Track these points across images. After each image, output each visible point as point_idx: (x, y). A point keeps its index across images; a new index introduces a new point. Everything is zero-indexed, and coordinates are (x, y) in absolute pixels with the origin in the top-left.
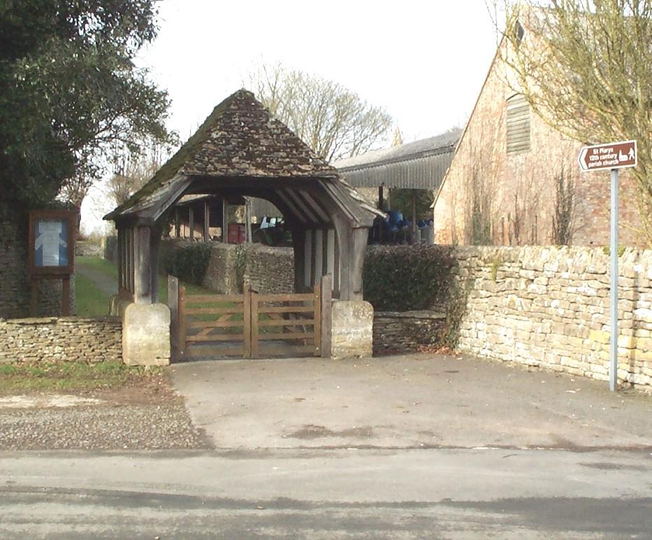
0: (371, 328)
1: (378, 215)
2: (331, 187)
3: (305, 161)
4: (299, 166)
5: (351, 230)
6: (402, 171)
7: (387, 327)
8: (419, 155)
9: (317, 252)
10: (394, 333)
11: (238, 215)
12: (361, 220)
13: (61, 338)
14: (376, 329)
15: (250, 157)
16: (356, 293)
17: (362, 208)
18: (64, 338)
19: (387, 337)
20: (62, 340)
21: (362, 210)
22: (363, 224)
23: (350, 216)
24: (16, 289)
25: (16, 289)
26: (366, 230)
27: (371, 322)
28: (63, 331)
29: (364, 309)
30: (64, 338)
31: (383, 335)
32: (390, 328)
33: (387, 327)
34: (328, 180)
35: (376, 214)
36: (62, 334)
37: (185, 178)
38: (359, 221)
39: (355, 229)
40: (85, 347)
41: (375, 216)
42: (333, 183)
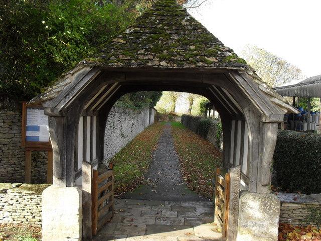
0: (278, 221)
1: (289, 111)
2: (239, 79)
3: (214, 55)
4: (206, 58)
5: (261, 124)
6: (304, 89)
7: (295, 212)
8: (313, 82)
9: (237, 142)
10: (300, 218)
11: (77, 110)
12: (270, 115)
13: (10, 205)
14: (283, 214)
15: (158, 50)
16: (265, 185)
17: (272, 102)
18: (12, 205)
19: (294, 221)
20: (10, 206)
21: (272, 105)
22: (273, 119)
23: (261, 112)
24: (19, 156)
25: (19, 156)
26: (276, 124)
27: (278, 216)
28: (12, 199)
29: (271, 204)
30: (12, 205)
31: (290, 219)
32: (297, 213)
33: (295, 212)
34: (236, 72)
35: (286, 108)
36: (11, 202)
37: (88, 69)
38: (268, 115)
39: (264, 123)
40: (28, 214)
41: (286, 111)
42: (240, 75)
